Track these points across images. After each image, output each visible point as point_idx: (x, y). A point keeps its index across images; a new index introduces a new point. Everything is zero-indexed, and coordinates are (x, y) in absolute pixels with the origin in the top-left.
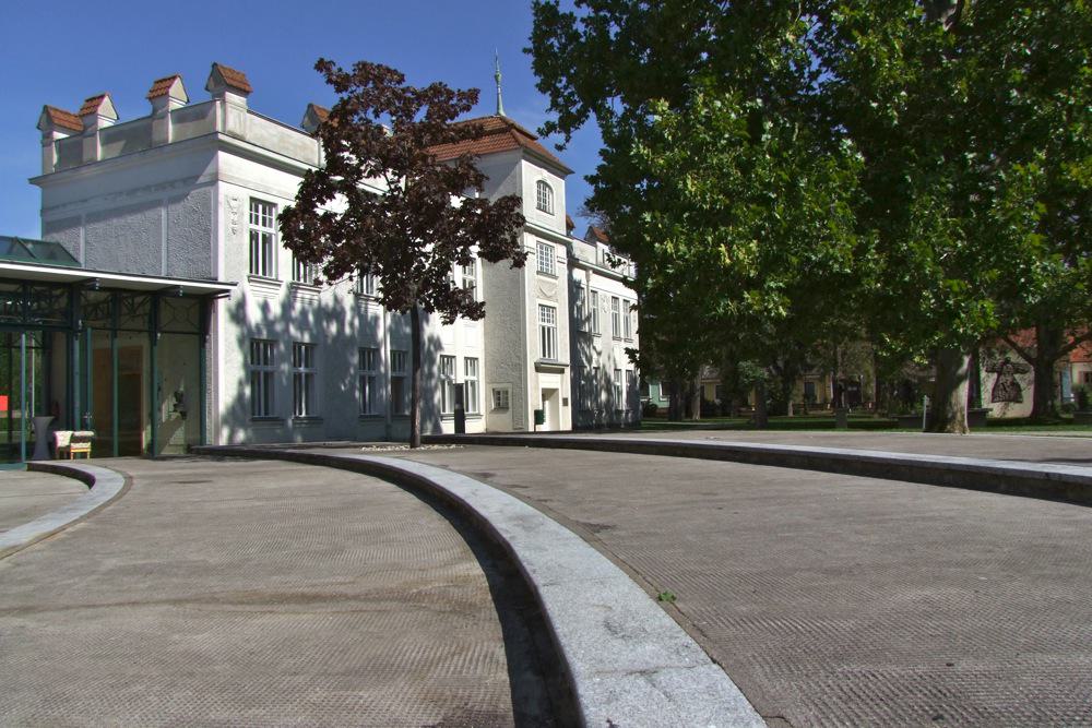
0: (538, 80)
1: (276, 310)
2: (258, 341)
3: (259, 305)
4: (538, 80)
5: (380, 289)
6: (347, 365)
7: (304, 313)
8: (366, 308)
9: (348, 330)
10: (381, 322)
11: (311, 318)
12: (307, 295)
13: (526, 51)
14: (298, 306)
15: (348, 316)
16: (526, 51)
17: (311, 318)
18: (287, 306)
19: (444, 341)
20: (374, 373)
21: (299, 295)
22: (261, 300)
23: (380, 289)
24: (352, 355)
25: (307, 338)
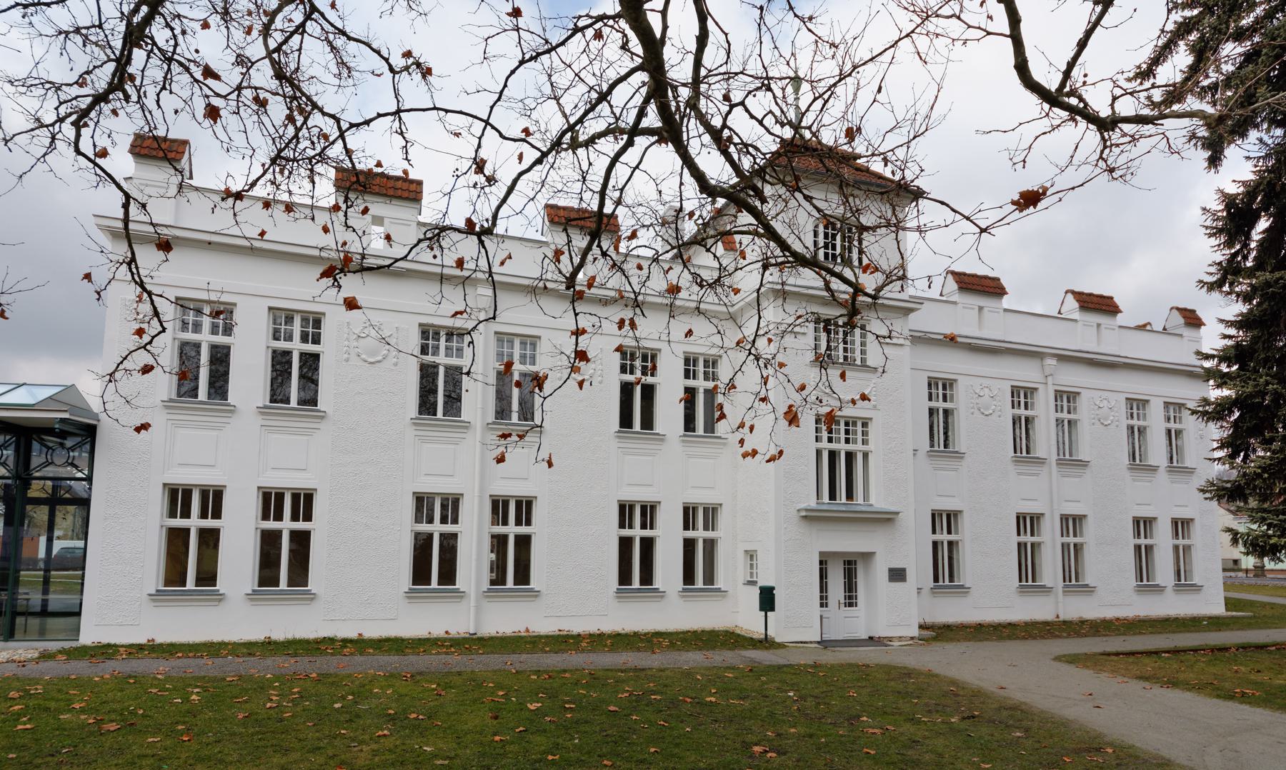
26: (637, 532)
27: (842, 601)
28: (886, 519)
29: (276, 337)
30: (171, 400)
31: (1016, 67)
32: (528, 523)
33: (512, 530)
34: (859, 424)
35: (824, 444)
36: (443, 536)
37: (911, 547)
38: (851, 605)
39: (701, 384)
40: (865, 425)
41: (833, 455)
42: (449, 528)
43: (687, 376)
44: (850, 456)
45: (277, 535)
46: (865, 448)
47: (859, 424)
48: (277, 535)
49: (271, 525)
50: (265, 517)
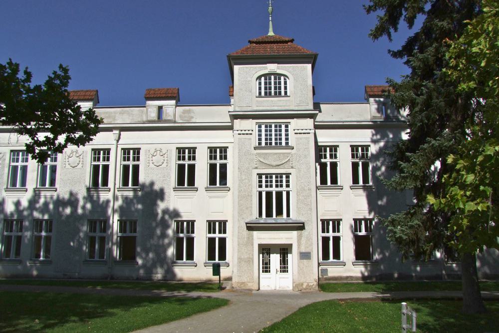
0: (408, 25)
1: (25, 203)
2: (12, 221)
3: (13, 203)
4: (408, 25)
5: (18, 204)
6: (79, 231)
7: (46, 204)
8: (98, 197)
9: (80, 211)
10: (111, 204)
11: (51, 206)
12: (49, 194)
13: (68, 66)
14: (42, 200)
15: (81, 203)
16: (68, 66)
17: (51, 206)
18: (33, 202)
19: (181, 210)
20: (104, 235)
21: (42, 194)
22: (15, 200)
23: (18, 204)
24: (83, 225)
25: (46, 217)
26: (217, 235)
27: (279, 269)
28: (300, 227)
29: (179, 159)
30: (175, 188)
31: (413, 24)
32: (339, 231)
33: (217, 235)
34: (284, 176)
35: (264, 189)
36: (220, 239)
37: (312, 240)
38: (284, 271)
39: (218, 162)
40: (288, 177)
41: (269, 194)
42: (222, 235)
43: (211, 158)
44: (279, 195)
45: (214, 239)
46: (288, 189)
47: (284, 176)
48: (214, 239)
49: (212, 235)
50: (210, 232)
